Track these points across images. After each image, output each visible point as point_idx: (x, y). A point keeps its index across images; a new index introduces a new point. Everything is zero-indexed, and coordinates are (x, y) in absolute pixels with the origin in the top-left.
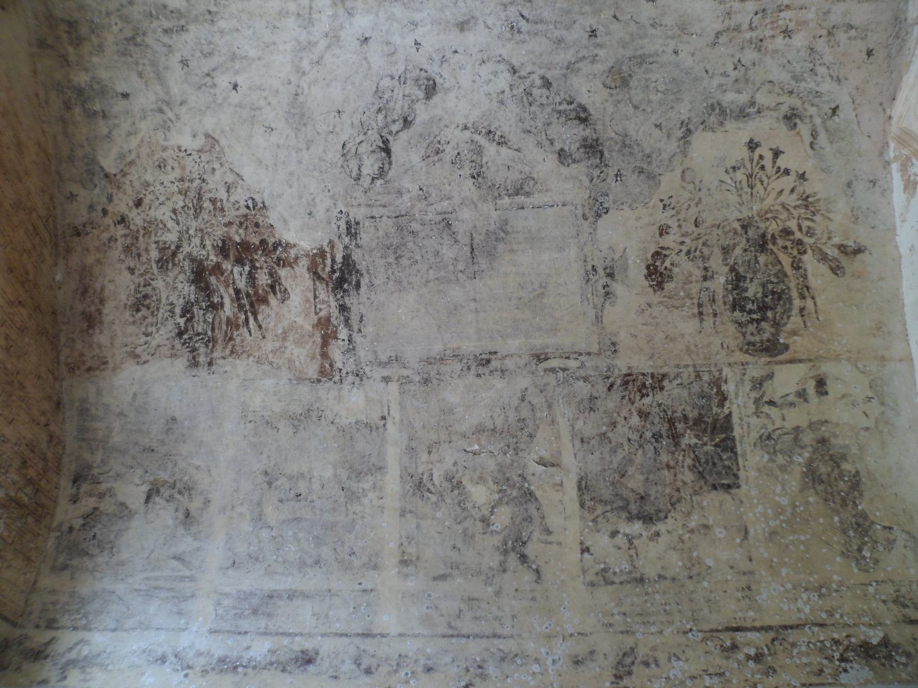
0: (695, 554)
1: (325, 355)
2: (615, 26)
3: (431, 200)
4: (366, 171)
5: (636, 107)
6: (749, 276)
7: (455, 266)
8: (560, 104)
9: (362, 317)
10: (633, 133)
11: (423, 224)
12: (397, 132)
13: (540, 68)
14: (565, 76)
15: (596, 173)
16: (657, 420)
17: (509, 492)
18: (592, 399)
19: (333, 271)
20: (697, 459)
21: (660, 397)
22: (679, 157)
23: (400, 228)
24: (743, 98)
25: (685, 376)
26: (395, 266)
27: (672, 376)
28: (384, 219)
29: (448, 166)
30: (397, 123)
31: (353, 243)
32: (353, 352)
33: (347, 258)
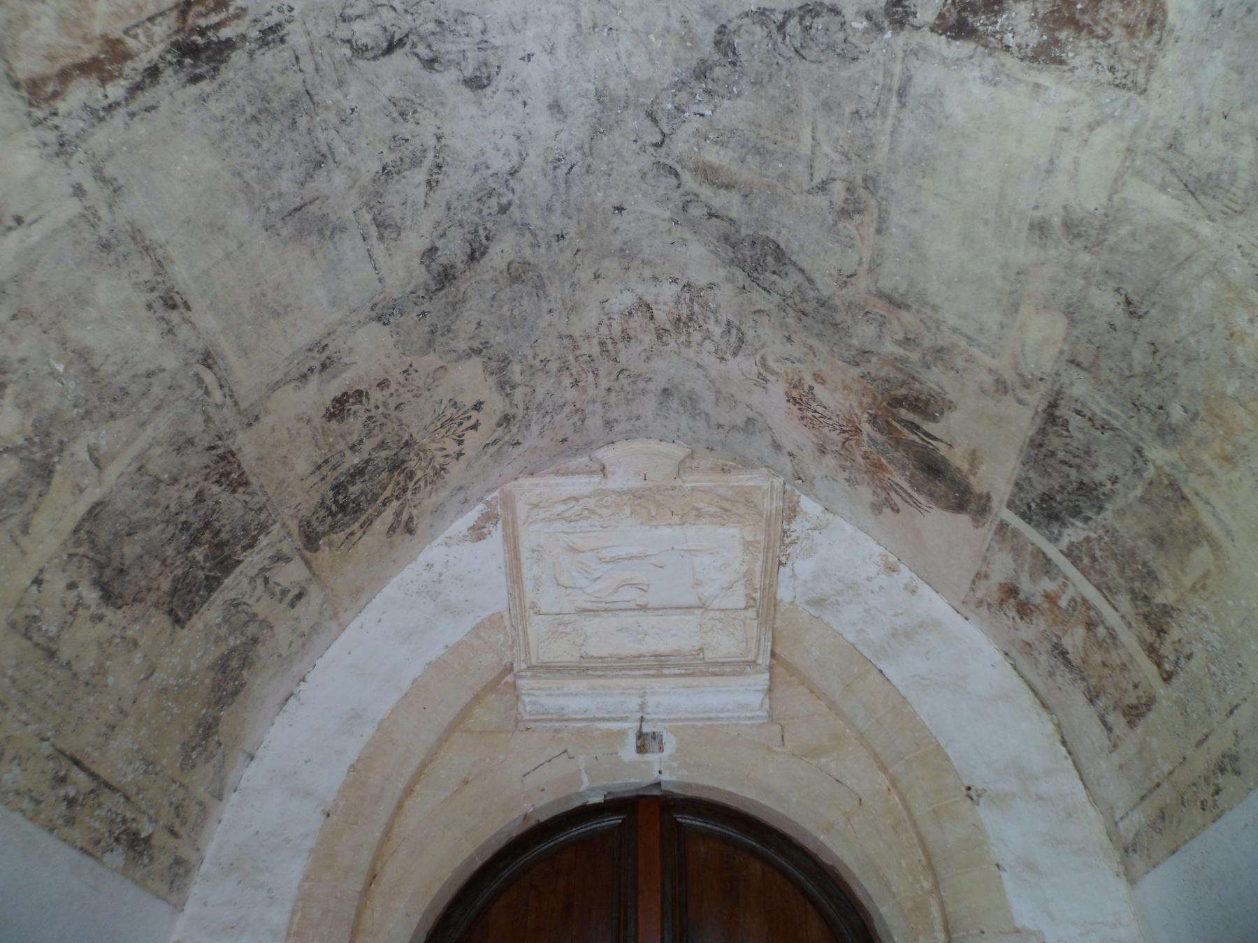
0: (108, 663)
1: (65, 76)
2: (569, 254)
3: (343, 128)
4: (357, 26)
5: (493, 298)
6: (366, 477)
7: (272, 199)
8: (485, 229)
9: (154, 108)
10: (468, 306)
11: (309, 131)
12: (417, 55)
13: (520, 199)
14: (515, 224)
15: (421, 293)
16: (200, 513)
17: (35, 449)
18: (190, 442)
19: (202, 33)
20: (186, 575)
21: (225, 497)
22: (454, 356)
23: (294, 103)
24: (517, 378)
25: (256, 499)
26: (242, 120)
27: (250, 490)
28: (300, 76)
29: (389, 133)
30: (427, 51)
31: (253, 46)
32: (95, 121)
33: (229, 45)
